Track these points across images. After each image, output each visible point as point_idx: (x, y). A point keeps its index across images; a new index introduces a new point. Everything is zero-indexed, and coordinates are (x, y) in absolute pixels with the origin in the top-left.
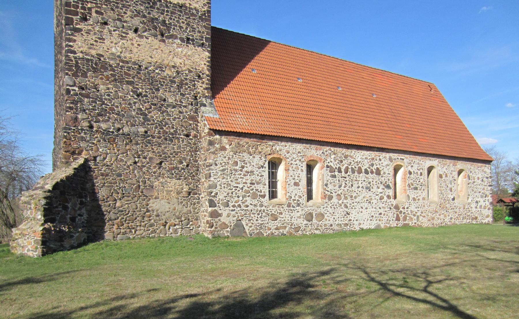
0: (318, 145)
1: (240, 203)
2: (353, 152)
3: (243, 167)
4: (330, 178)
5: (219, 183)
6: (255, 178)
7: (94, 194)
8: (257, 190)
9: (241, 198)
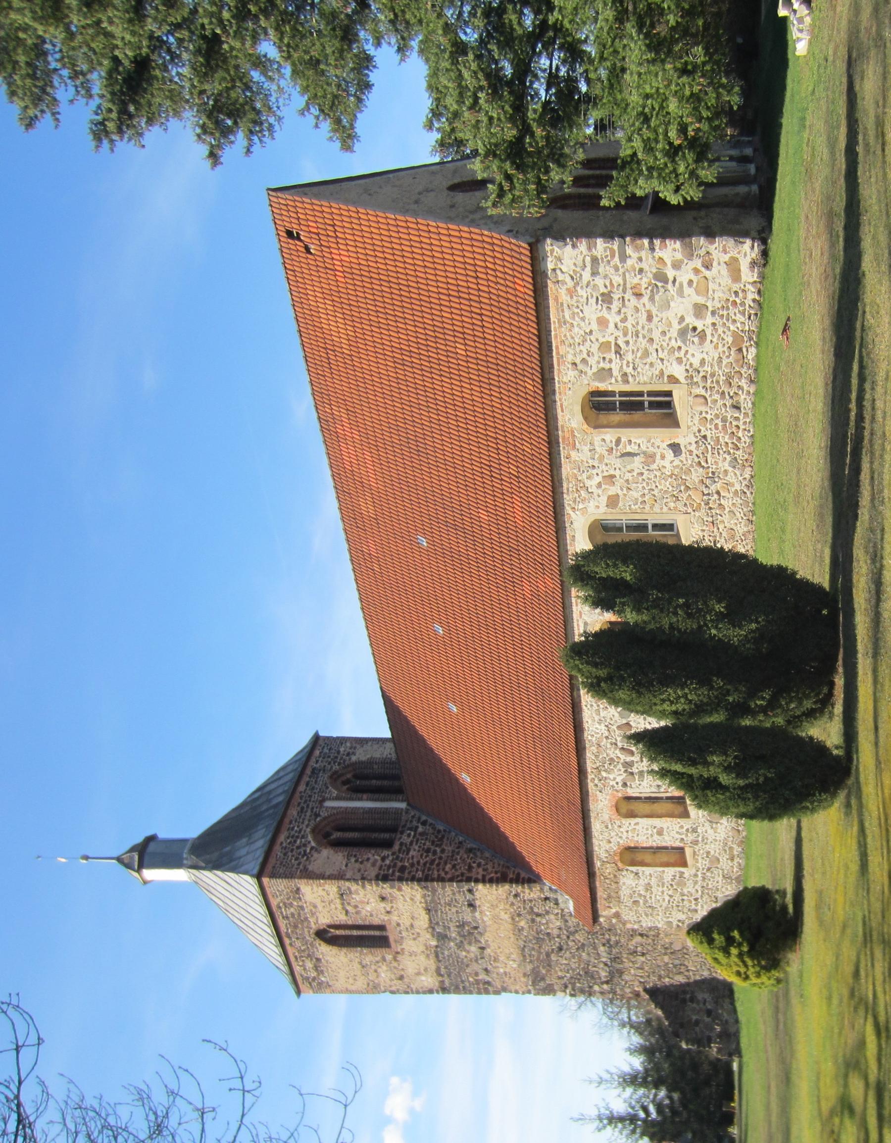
0: (589, 817)
1: (692, 899)
2: (590, 738)
3: (640, 895)
4: (645, 781)
5: (665, 919)
6: (654, 882)
7: (682, 985)
8: (672, 880)
9: (685, 898)
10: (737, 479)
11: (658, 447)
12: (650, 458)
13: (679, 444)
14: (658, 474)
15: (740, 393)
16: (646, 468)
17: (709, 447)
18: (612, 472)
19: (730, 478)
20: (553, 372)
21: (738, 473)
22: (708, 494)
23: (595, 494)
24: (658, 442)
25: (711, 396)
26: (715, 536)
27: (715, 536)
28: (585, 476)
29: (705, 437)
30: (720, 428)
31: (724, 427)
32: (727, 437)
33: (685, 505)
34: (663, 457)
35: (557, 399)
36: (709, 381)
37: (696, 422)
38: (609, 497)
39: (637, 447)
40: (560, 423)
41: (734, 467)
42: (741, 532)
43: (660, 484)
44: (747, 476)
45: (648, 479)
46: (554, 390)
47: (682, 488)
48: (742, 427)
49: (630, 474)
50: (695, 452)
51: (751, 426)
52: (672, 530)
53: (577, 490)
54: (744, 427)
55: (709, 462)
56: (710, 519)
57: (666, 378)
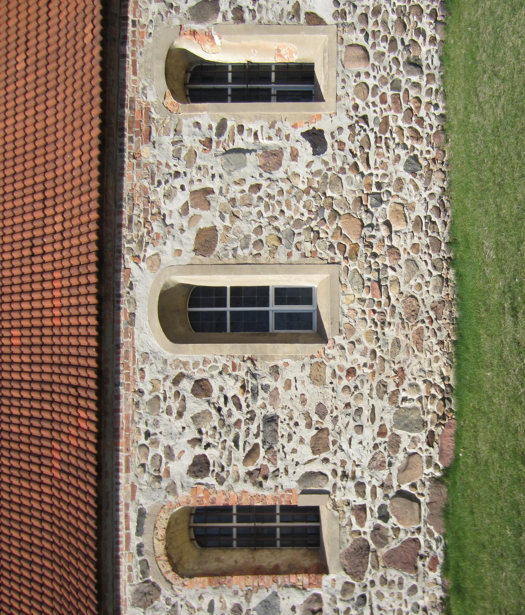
10: (420, 197)
11: (288, 137)
12: (272, 158)
13: (321, 132)
14: (286, 186)
15: (420, 40)
16: (266, 175)
17: (372, 136)
18: (208, 183)
19: (408, 195)
20: (127, 6)
21: (420, 184)
22: (371, 226)
23: (177, 228)
24: (287, 128)
25: (374, 45)
26: (383, 313)
27: (383, 313)
28: (161, 191)
29: (365, 118)
30: (389, 100)
31: (396, 98)
32: (400, 116)
33: (331, 246)
34: (294, 156)
35: (129, 53)
36: (371, 21)
37: (350, 91)
38: (200, 233)
39: (251, 139)
40: (129, 94)
41: (414, 173)
42: (429, 302)
43: (289, 206)
44: (436, 190)
45: (269, 196)
46: (125, 37)
47: (327, 213)
48: (425, 99)
49: (238, 188)
50: (349, 145)
51: (440, 96)
52: (309, 326)
53: (146, 221)
54: (427, 99)
55: (372, 163)
56: (374, 276)
57: (303, 16)
